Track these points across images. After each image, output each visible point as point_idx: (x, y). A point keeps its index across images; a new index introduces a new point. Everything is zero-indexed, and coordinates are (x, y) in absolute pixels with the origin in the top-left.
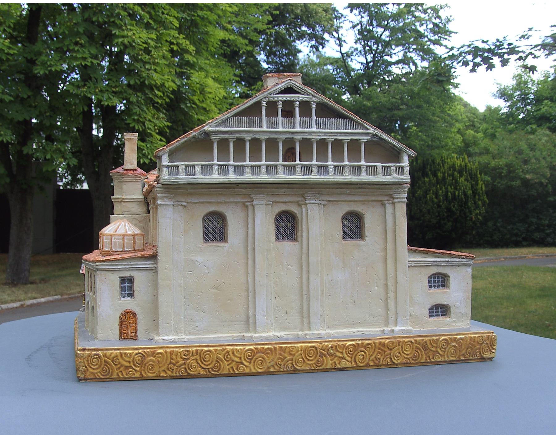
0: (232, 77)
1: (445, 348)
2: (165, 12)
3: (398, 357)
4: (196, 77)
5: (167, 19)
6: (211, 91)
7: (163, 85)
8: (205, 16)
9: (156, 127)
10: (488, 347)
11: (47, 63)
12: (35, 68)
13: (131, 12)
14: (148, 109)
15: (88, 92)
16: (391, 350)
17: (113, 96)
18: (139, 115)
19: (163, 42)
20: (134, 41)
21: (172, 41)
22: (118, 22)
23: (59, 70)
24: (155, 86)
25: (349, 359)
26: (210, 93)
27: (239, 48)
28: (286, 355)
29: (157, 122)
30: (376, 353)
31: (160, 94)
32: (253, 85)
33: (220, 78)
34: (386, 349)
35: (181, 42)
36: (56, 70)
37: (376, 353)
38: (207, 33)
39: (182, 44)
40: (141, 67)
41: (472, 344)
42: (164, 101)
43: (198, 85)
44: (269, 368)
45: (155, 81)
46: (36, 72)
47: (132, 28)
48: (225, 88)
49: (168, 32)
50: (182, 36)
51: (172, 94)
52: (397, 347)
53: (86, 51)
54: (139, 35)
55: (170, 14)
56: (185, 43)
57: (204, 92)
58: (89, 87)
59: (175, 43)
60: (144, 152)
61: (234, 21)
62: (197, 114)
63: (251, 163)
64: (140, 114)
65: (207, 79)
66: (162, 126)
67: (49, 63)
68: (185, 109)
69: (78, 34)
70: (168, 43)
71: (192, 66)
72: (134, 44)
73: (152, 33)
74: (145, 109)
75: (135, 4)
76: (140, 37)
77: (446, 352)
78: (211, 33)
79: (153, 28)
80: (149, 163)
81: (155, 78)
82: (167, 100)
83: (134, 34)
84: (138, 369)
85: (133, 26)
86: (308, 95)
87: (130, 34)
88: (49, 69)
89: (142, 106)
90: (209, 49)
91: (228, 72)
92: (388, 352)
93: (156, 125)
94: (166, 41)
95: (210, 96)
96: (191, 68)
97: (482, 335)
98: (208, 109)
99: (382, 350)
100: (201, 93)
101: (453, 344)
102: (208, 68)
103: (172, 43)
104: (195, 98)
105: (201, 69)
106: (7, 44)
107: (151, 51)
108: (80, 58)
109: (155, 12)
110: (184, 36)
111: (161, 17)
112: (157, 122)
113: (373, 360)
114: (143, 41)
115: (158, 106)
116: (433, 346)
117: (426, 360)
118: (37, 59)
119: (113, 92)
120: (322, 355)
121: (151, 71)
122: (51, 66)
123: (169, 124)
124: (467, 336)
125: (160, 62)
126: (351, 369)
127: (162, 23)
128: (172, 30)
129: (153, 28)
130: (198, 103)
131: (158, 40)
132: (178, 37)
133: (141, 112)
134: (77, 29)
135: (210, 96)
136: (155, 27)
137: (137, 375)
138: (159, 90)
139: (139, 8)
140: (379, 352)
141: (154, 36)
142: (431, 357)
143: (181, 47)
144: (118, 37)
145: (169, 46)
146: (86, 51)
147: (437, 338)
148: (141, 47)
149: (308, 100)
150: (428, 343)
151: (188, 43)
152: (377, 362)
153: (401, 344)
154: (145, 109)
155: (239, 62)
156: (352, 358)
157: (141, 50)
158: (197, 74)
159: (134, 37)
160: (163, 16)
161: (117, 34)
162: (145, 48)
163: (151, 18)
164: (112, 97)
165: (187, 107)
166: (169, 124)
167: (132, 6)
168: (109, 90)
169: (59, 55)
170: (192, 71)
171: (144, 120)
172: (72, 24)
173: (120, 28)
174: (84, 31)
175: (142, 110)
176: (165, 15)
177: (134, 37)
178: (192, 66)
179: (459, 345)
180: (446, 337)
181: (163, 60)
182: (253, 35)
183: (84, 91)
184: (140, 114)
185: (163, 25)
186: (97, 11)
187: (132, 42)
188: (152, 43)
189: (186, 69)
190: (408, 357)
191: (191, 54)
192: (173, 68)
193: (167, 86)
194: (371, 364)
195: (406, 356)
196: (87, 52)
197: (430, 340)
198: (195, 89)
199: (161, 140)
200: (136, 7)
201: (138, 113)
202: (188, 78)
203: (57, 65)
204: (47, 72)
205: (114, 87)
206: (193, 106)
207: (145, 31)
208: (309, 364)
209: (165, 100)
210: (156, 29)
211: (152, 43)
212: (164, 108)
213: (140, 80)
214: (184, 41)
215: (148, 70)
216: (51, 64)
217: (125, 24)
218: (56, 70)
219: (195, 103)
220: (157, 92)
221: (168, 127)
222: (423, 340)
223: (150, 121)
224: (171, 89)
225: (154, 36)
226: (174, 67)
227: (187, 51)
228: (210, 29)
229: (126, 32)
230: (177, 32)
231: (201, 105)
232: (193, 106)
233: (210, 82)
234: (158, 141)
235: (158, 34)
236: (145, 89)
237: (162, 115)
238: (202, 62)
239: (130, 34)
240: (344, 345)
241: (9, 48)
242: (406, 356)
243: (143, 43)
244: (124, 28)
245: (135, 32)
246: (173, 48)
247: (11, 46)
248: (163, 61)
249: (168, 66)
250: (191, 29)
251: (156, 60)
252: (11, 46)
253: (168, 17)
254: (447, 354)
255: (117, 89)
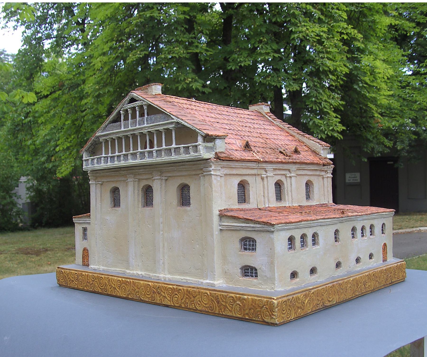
0: (401, 58)
1: (232, 305)
2: (335, 7)
3: (199, 305)
4: (366, 61)
5: (336, 13)
6: (380, 71)
7: (336, 70)
8: (371, 7)
9: (332, 106)
10: (268, 312)
11: (237, 60)
12: (228, 64)
13: (304, 11)
14: (324, 91)
15: (272, 81)
16: (194, 297)
17: (294, 83)
18: (316, 97)
19: (335, 33)
20: (308, 35)
21: (342, 31)
22: (293, 20)
23: (247, 65)
24: (330, 71)
25: (169, 299)
26: (380, 73)
27: (406, 31)
28: (136, 288)
29: (333, 102)
30: (185, 298)
31: (334, 78)
32: (422, 63)
33: (390, 59)
34: (191, 296)
35: (350, 32)
36: (245, 65)
37: (185, 298)
38: (374, 22)
39: (351, 34)
40: (316, 57)
41: (253, 306)
42: (338, 84)
43: (368, 67)
44: (128, 295)
45: (328, 67)
46: (229, 68)
47: (306, 24)
48: (394, 67)
49: (338, 24)
50: (350, 26)
51: (345, 77)
52: (198, 296)
53: (268, 47)
54: (313, 30)
55: (340, 8)
56: (354, 32)
57: (375, 72)
58: (273, 77)
59: (345, 33)
60: (321, 128)
61: (401, 8)
62: (369, 92)
63: (167, 147)
64: (316, 96)
65: (375, 62)
66: (337, 105)
67: (239, 60)
68: (358, 89)
69: (261, 34)
70: (338, 34)
71: (362, 51)
72: (308, 38)
73: (324, 27)
74: (321, 91)
75: (307, 4)
76: (312, 31)
77: (233, 309)
78: (378, 21)
79: (324, 22)
80: (326, 138)
81: (329, 65)
82: (342, 82)
83: (307, 29)
84: (76, 283)
85: (307, 22)
86: (141, 101)
87: (304, 29)
88: (239, 64)
89: (319, 90)
90: (378, 35)
91: (397, 53)
92: (192, 299)
93: (331, 105)
94: (337, 32)
95: (380, 75)
96: (362, 53)
97: (263, 299)
98: (378, 88)
99: (189, 296)
100: (371, 74)
101: (238, 302)
102: (376, 51)
103: (341, 33)
104: (367, 79)
105: (371, 53)
106: (204, 48)
107: (324, 42)
108: (264, 53)
109: (325, 8)
110: (352, 26)
111: (331, 12)
112: (333, 102)
113: (183, 303)
114: (316, 34)
115: (334, 88)
116: (223, 301)
117: (219, 312)
118: (229, 58)
119: (294, 79)
120: (154, 292)
121: (324, 59)
122: (240, 62)
123: (344, 103)
124: (250, 297)
125: (332, 50)
126: (205, 313)
127: (331, 17)
128: (340, 22)
129: (324, 22)
130: (369, 83)
131: (330, 31)
132: (347, 28)
133: (318, 95)
134: (260, 30)
135: (380, 75)
136: (326, 21)
137: (76, 287)
138: (333, 75)
139: (311, 7)
140: (187, 298)
141: (325, 29)
142: (223, 310)
143: (350, 36)
144: (295, 33)
145: (341, 36)
146: (268, 47)
147: (226, 294)
148: (314, 39)
149: (141, 104)
150: (219, 297)
151: (356, 31)
152: (186, 305)
153: (200, 294)
154: (321, 91)
155: (411, 44)
156: (170, 298)
157: (315, 42)
158: (367, 57)
159: (307, 32)
160: (333, 11)
161: (293, 30)
162: (318, 40)
163: (322, 14)
164: (292, 84)
165: (359, 87)
166: (344, 103)
167: (304, 6)
168: (290, 78)
169: (247, 53)
170: (362, 56)
171: (321, 101)
172: (256, 26)
173: (295, 25)
174: (266, 30)
175: (319, 93)
176: (334, 10)
177: (307, 32)
178: (362, 51)
179: (243, 304)
180: (233, 295)
181: (334, 48)
182: (420, 18)
183: (268, 80)
184: (316, 96)
185: (334, 18)
186: (276, 13)
187: (306, 36)
188: (325, 35)
189: (357, 54)
190: (207, 306)
191: (359, 41)
192: (344, 55)
193: (339, 71)
194: (183, 306)
195: (204, 305)
196: (269, 48)
197: (220, 295)
198: (365, 71)
199: (336, 117)
200: (308, 6)
201: (315, 95)
202: (359, 62)
203: (246, 61)
204: (238, 67)
205: (294, 75)
206: (365, 85)
207: (317, 25)
208: (148, 298)
209: (339, 82)
210: (327, 23)
211: (325, 35)
212: (339, 90)
213: (315, 67)
214: (352, 30)
215: (322, 58)
216: (240, 60)
217: (300, 21)
218: (245, 65)
219: (366, 83)
220: (331, 76)
221: (342, 105)
222: (216, 294)
223: (326, 101)
224: (344, 73)
225: (325, 29)
226: (346, 54)
227: (355, 39)
228: (377, 17)
229: (300, 29)
230: (345, 23)
231: (372, 84)
232: (365, 85)
233: (378, 63)
234: (334, 118)
235: (330, 27)
236: (321, 74)
237: (336, 96)
238: (371, 47)
239: (304, 29)
240: (166, 287)
241: (207, 51)
242: (204, 305)
243: (316, 36)
244: (299, 25)
245: (308, 27)
246: (343, 37)
247: (208, 49)
248: (335, 50)
249: (340, 53)
250: (361, 19)
251: (328, 50)
252: (208, 49)
253: (337, 11)
254: (234, 311)
255: (297, 76)
